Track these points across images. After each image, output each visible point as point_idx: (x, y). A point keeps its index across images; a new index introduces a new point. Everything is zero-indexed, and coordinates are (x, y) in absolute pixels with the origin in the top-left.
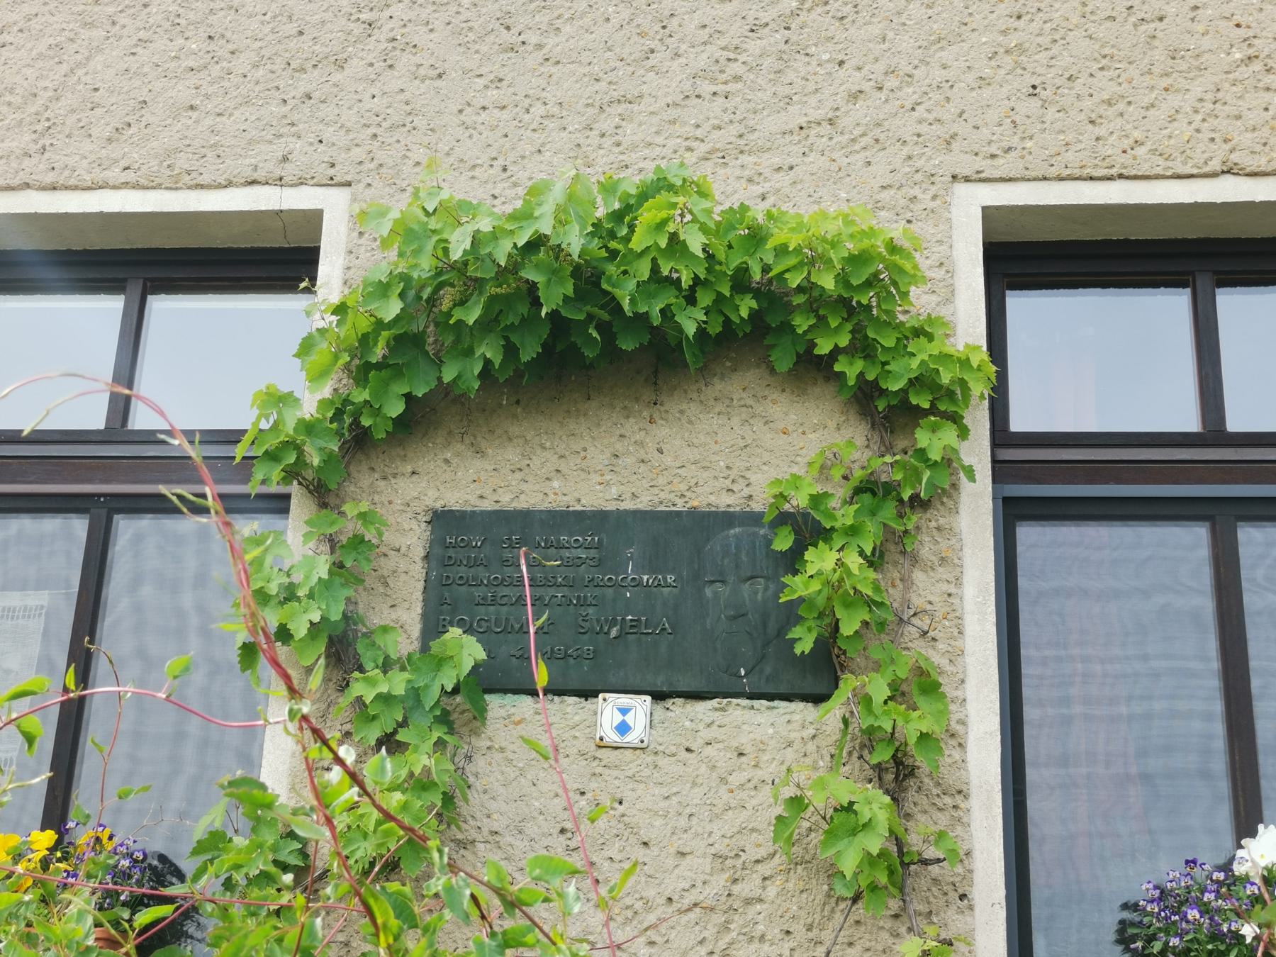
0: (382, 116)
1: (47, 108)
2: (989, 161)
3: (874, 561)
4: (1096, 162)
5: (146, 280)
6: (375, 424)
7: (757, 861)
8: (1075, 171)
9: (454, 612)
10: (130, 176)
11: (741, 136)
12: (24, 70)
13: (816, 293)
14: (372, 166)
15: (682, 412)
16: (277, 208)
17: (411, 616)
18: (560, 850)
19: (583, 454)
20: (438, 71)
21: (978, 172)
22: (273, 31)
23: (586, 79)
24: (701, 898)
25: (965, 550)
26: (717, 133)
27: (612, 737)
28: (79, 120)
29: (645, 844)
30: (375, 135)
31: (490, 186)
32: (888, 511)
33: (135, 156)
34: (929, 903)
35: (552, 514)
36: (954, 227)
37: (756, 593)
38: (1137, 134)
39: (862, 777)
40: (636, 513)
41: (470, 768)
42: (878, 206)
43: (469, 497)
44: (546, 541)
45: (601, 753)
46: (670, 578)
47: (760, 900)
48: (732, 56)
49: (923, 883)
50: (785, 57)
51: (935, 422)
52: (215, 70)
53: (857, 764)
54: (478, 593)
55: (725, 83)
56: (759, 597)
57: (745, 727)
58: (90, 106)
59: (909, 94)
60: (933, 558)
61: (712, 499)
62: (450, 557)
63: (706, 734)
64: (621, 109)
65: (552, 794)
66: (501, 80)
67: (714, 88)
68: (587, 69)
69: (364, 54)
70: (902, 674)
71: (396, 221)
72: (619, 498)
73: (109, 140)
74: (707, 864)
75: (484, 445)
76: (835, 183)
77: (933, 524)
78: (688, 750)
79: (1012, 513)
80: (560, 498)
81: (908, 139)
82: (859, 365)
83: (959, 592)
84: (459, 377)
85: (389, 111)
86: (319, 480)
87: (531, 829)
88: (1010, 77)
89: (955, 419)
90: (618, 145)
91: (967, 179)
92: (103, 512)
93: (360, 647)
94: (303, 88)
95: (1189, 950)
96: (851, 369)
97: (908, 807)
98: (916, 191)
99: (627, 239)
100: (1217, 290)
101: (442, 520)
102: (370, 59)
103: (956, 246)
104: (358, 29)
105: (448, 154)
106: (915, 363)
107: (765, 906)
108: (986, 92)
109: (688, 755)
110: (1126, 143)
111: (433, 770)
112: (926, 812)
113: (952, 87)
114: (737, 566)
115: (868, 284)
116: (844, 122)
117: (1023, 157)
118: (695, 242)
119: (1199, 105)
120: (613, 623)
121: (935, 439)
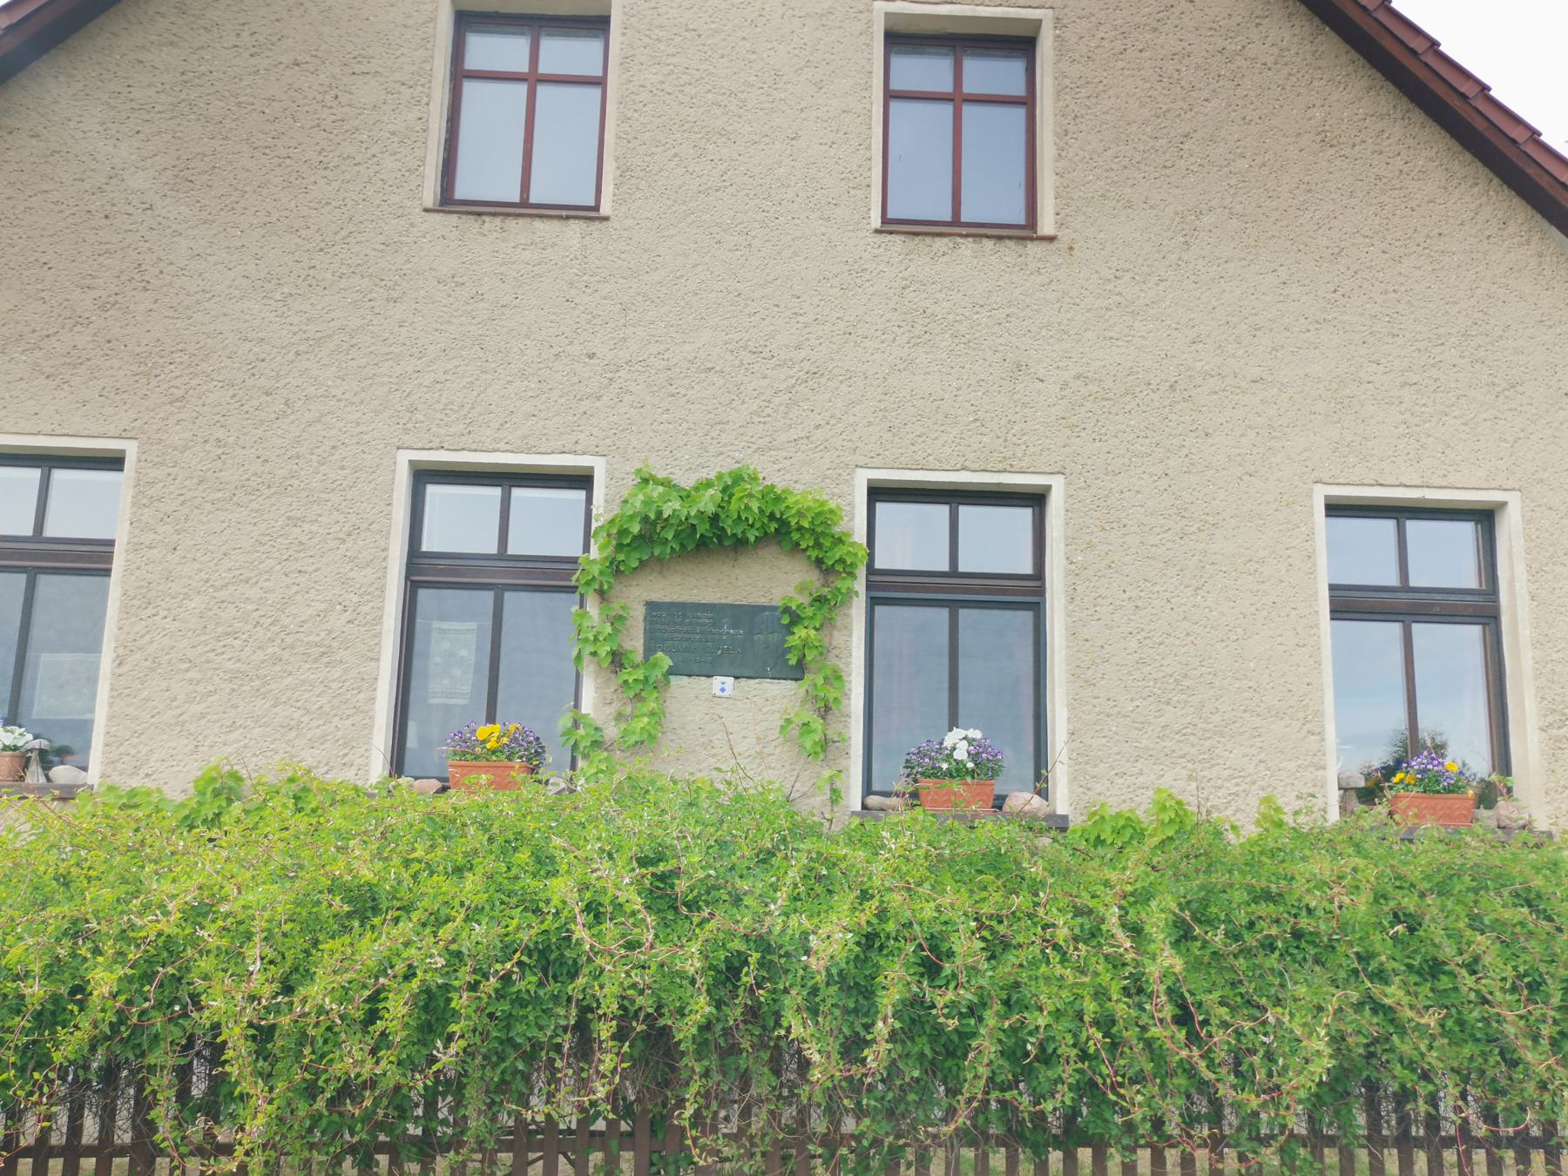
10: (508, 447)
27: (719, 693)
74: (754, 741)
79: (873, 602)
101: (651, 605)
104: (606, 382)
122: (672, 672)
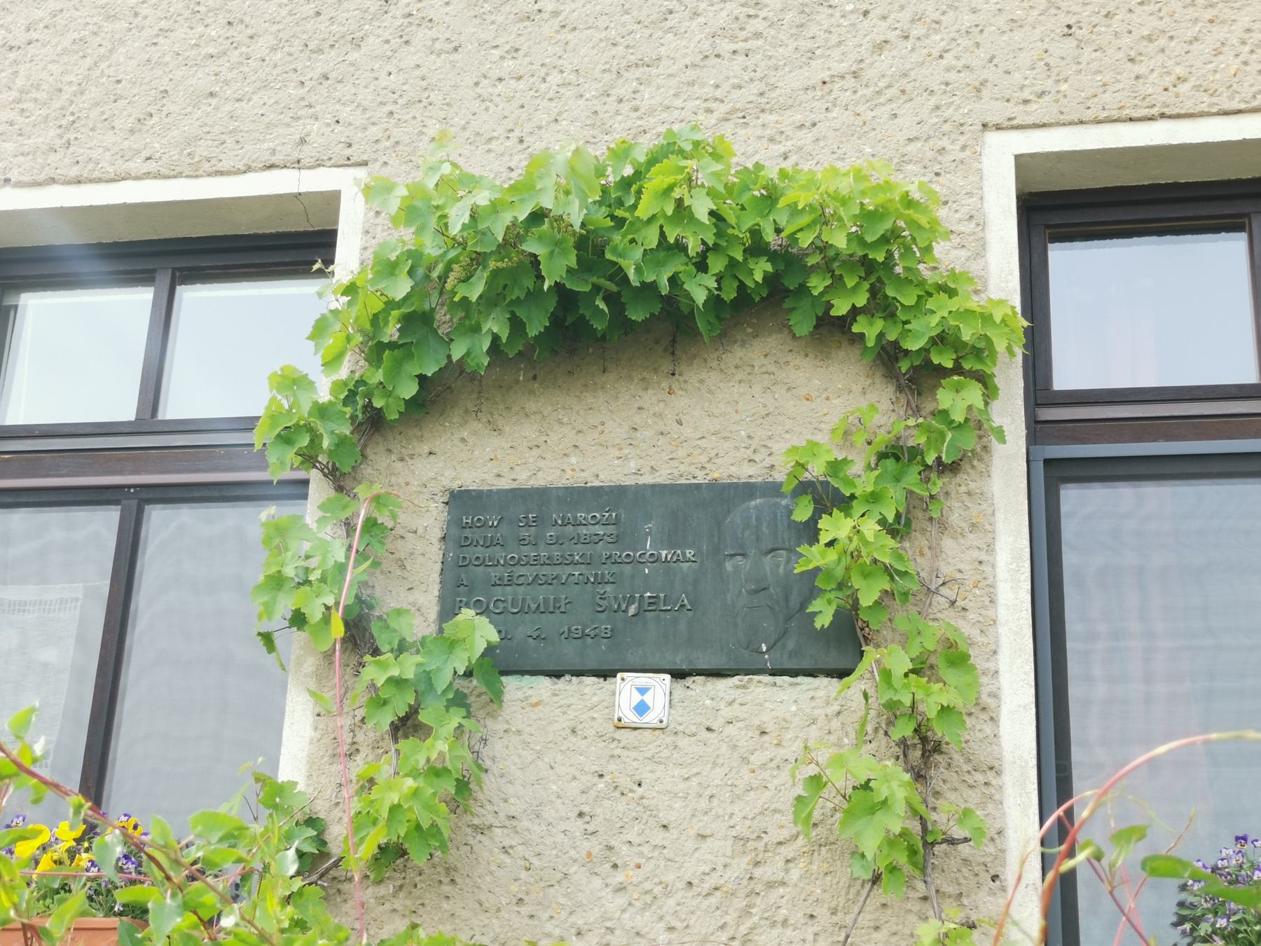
0: (399, 93)
1: (72, 102)
2: (1021, 107)
3: (896, 529)
4: (1136, 101)
5: (174, 269)
6: (387, 405)
7: (780, 843)
8: (1113, 113)
9: (470, 593)
10: (152, 166)
11: (762, 94)
12: (50, 66)
13: (831, 253)
14: (388, 144)
15: (701, 381)
16: (295, 191)
17: (428, 598)
18: (578, 834)
19: (600, 428)
20: (454, 45)
21: (1010, 119)
22: (291, 14)
23: (602, 45)
24: (722, 882)
25: (997, 514)
26: (736, 94)
27: (630, 717)
28: (103, 113)
29: (665, 826)
30: (391, 113)
31: (506, 158)
32: (912, 478)
33: (157, 145)
34: (959, 884)
35: (568, 490)
36: (985, 177)
37: (778, 566)
38: (1179, 71)
39: (889, 754)
40: (653, 487)
41: (486, 752)
42: (904, 160)
43: (486, 476)
44: (563, 518)
45: (620, 734)
46: (689, 553)
47: (783, 884)
48: (752, 12)
49: (953, 864)
50: (807, 10)
51: (958, 382)
52: (235, 56)
53: (884, 740)
54: (494, 573)
55: (746, 40)
56: (781, 570)
57: (767, 704)
58: (113, 98)
59: (937, 41)
60: (963, 525)
61: (733, 470)
62: (466, 538)
63: (726, 713)
64: (638, 73)
65: (570, 777)
66: (517, 50)
67: (734, 47)
68: (604, 34)
69: (380, 31)
70: (931, 646)
71: (403, 198)
72: (638, 472)
73: (132, 131)
75: (500, 422)
76: (859, 138)
77: (963, 489)
78: (708, 729)
79: (1052, 476)
80: (577, 474)
81: (936, 88)
82: (879, 325)
83: (991, 559)
84: (468, 354)
85: (405, 88)
86: (334, 464)
87: (549, 814)
88: (1043, 17)
89: (983, 379)
90: (636, 110)
91: (998, 128)
92: (135, 503)
93: (375, 628)
94: (320, 69)
95: (1238, 931)
96: (869, 329)
97: (936, 783)
98: (945, 142)
99: (635, 206)
100: (1050, 246)
101: (460, 500)
102: (386, 35)
103: (986, 196)
105: (464, 128)
106: (934, 320)
107: (788, 889)
108: (1018, 35)
109: (709, 734)
110: (1168, 81)
111: (448, 756)
112: (956, 789)
113: (982, 31)
114: (758, 539)
115: (885, 240)
116: (869, 74)
117: (1057, 101)
118: (701, 208)
119: (1247, 36)
120: (631, 600)
121: (958, 400)
122: (501, 663)
